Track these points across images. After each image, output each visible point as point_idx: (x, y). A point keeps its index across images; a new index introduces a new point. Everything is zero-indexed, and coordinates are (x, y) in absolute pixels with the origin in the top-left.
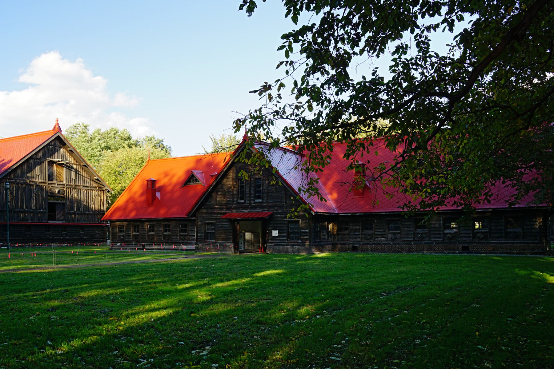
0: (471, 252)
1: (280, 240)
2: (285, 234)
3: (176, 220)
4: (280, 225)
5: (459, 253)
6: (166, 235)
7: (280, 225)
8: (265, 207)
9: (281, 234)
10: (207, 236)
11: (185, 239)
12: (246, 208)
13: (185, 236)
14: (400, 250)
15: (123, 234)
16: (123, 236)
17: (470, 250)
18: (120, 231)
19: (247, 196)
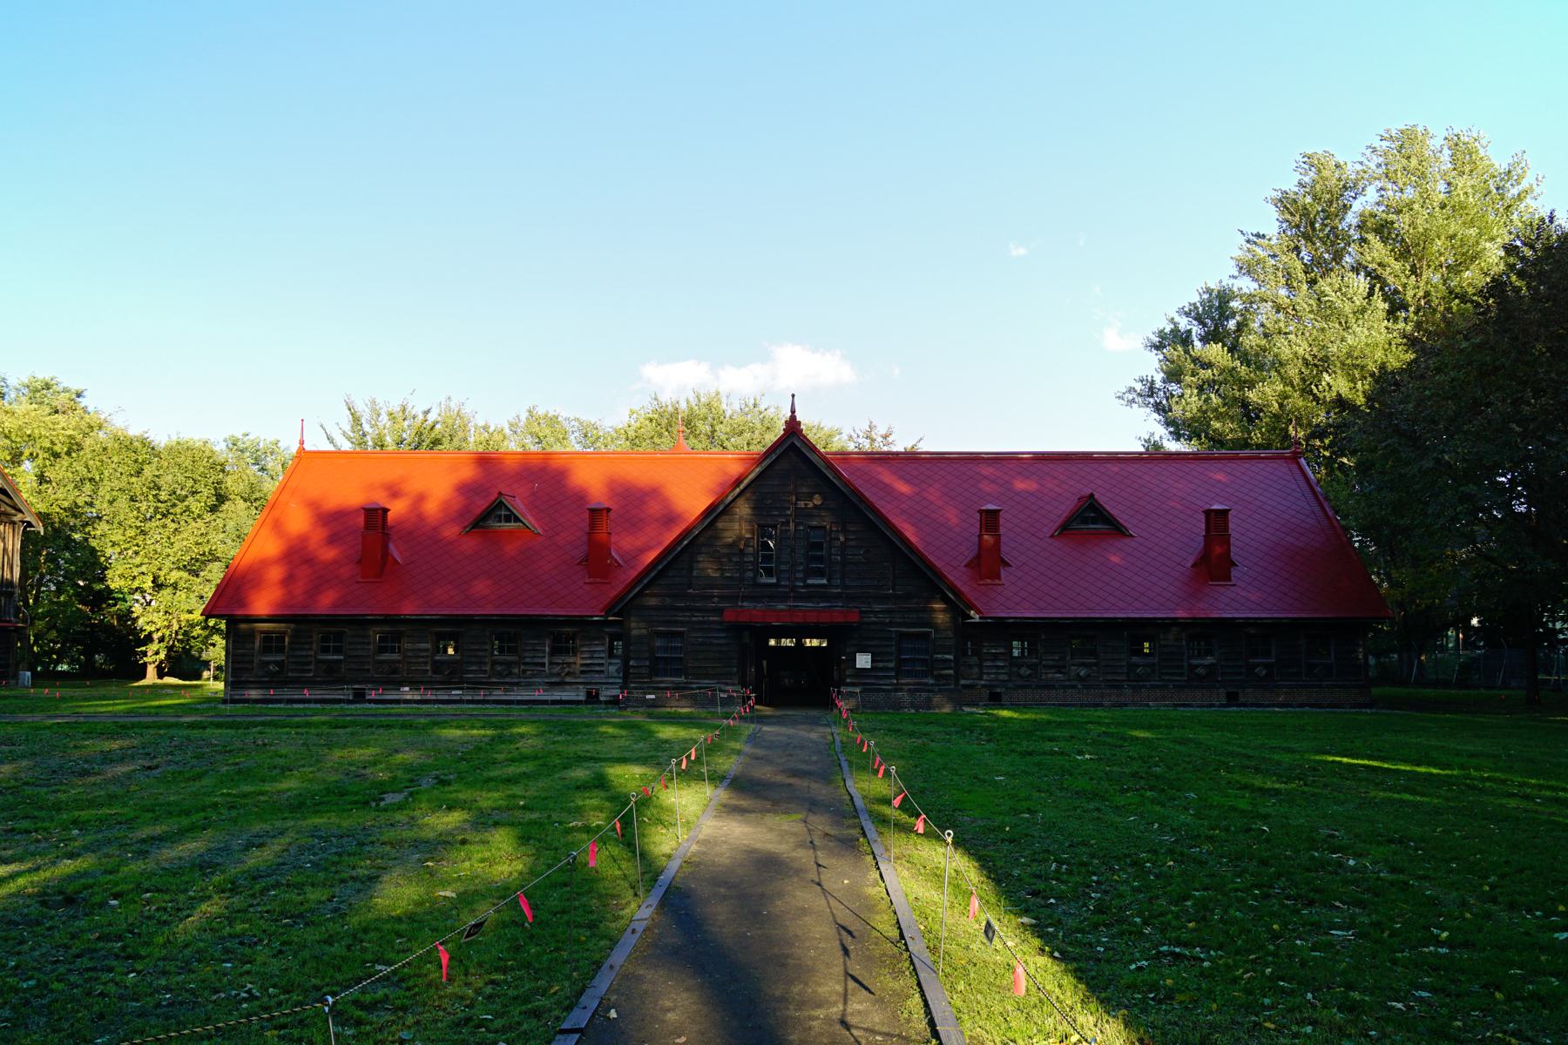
0: (1245, 705)
1: (877, 677)
2: (892, 665)
3: (486, 621)
4: (876, 642)
5: (1222, 706)
6: (382, 662)
7: (876, 642)
8: (838, 597)
9: (881, 665)
10: (659, 666)
11: (510, 674)
12: (784, 598)
13: (509, 664)
14: (1098, 700)
15: (279, 658)
16: (280, 664)
17: (1242, 700)
18: (266, 649)
19: (783, 567)
